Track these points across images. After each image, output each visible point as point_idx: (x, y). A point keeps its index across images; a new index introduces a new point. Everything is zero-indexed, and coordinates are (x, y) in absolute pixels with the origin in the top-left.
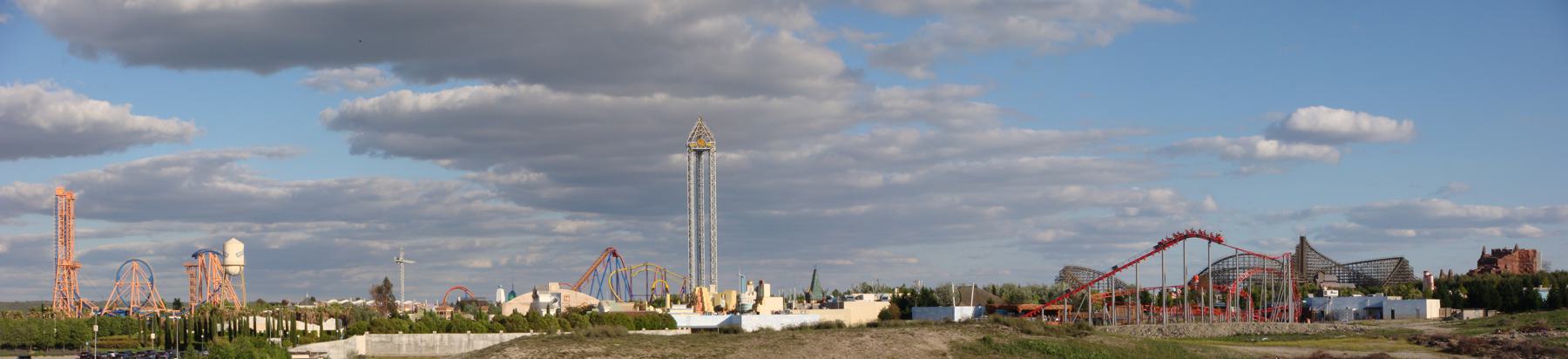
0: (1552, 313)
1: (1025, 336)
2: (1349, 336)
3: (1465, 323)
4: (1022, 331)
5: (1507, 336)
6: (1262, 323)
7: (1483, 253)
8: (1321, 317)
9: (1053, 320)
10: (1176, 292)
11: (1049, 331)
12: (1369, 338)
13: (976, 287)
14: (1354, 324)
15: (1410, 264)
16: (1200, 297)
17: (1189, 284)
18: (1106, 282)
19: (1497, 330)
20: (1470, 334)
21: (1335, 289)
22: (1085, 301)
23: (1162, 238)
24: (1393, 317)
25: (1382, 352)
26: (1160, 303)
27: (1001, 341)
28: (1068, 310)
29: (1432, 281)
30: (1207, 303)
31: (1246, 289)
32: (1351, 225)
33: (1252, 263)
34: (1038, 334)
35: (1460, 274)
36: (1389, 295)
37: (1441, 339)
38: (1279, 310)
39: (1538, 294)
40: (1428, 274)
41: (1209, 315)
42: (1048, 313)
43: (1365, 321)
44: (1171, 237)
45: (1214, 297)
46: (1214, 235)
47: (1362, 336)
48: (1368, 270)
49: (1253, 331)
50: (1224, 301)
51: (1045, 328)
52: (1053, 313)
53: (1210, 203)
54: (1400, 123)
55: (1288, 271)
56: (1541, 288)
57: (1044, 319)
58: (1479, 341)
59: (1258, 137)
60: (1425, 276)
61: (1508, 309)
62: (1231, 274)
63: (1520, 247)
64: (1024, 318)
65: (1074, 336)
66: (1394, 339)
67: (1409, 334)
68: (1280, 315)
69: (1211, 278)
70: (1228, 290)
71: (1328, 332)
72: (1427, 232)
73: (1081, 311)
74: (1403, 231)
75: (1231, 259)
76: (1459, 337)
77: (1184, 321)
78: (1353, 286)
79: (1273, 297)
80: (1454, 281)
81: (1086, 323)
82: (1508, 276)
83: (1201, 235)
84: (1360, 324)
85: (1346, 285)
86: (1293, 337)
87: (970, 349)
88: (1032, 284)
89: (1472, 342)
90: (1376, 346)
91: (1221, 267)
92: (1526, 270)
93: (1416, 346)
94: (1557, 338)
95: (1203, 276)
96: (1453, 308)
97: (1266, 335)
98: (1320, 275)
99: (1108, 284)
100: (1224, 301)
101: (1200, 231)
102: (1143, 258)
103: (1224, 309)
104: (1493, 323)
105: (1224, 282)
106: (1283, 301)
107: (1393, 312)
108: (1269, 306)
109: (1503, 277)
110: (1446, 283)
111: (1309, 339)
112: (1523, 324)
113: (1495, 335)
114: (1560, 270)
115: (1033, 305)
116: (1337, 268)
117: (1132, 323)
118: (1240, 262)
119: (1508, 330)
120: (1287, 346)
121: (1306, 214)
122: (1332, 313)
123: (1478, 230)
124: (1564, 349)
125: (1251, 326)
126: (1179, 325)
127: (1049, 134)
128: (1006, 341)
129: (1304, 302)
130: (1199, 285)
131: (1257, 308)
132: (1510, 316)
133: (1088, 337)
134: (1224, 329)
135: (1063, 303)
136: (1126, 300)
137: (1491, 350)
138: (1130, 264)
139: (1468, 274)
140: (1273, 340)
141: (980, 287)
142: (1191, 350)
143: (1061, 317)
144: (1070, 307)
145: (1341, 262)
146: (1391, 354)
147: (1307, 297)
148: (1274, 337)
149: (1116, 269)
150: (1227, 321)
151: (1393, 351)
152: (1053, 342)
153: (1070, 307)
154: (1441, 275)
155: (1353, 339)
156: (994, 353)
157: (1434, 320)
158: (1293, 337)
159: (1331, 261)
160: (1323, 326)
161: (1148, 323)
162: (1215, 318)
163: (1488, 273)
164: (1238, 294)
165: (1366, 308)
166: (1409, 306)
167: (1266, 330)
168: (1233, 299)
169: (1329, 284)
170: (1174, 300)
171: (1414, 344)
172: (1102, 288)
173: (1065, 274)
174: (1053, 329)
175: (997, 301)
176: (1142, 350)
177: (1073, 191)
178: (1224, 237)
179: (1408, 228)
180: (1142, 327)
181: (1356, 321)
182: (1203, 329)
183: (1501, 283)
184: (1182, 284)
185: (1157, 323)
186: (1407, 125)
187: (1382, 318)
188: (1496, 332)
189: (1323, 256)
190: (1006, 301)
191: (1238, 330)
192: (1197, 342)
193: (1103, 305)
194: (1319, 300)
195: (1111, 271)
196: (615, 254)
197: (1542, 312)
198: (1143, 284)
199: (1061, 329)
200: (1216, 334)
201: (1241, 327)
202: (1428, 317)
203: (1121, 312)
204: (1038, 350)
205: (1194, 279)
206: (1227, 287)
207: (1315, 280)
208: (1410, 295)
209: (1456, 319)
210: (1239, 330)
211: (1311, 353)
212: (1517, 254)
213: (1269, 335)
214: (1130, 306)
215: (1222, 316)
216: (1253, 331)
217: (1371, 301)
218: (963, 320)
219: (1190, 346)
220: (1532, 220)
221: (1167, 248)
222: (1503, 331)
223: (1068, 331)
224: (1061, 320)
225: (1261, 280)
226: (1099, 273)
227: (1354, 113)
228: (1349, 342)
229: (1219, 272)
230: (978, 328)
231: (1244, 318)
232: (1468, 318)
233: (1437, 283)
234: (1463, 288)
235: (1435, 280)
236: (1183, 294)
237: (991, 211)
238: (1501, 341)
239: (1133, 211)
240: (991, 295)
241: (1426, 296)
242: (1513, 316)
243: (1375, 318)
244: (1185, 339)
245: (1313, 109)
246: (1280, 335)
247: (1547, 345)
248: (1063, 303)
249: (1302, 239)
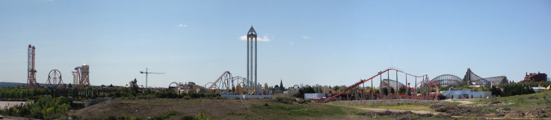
75: (441, 77)
102: (374, 77)
107: (472, 96)
196: (229, 73)
226: (481, 78)
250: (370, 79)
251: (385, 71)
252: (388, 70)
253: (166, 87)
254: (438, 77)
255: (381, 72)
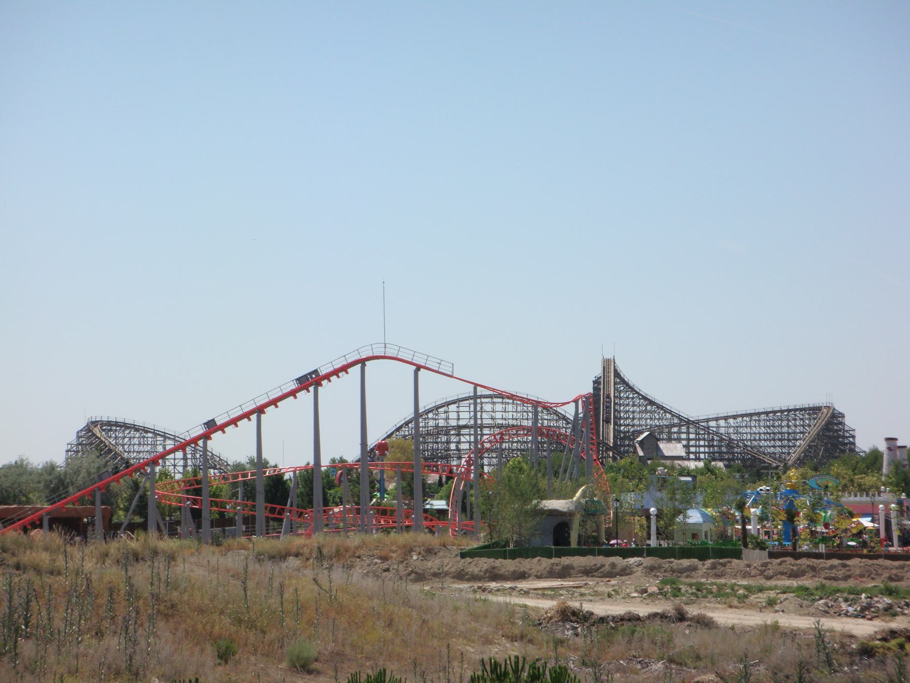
75: (453, 407)
102: (274, 402)
226: (679, 417)
250: (247, 415)
251: (345, 368)
252: (362, 362)
253: (37, 459)
254: (438, 408)
255: (316, 372)
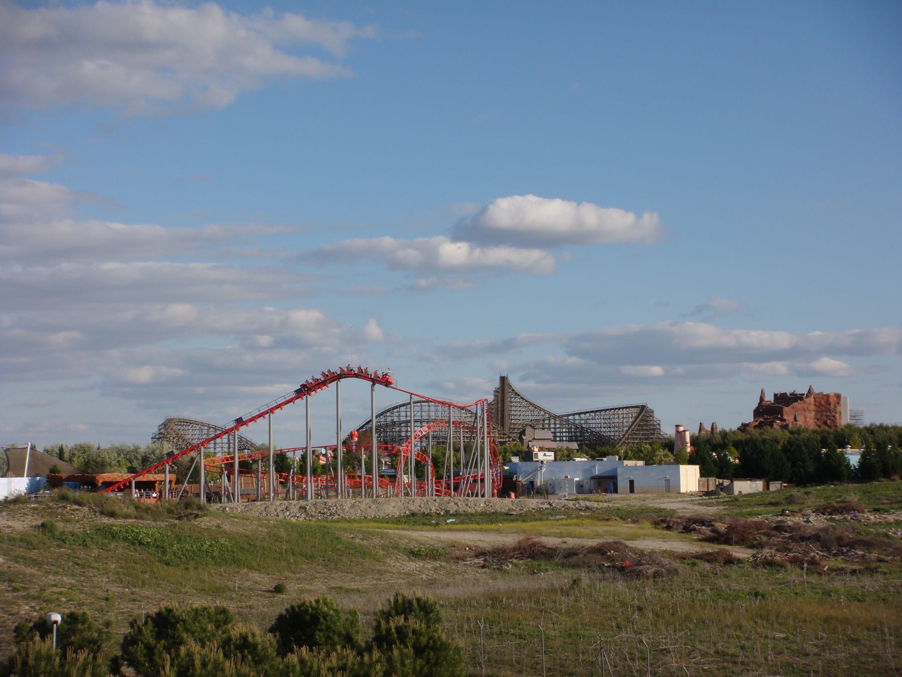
0: (867, 486)
1: (106, 520)
2: (569, 516)
3: (736, 500)
4: (102, 513)
5: (798, 519)
6: (447, 498)
7: (762, 399)
8: (531, 489)
9: (148, 496)
10: (325, 455)
11: (142, 511)
12: (598, 519)
13: (33, 448)
14: (576, 500)
15: (655, 414)
16: (360, 461)
17: (344, 443)
18: (226, 441)
19: (783, 511)
20: (743, 515)
21: (549, 450)
22: (195, 468)
23: (307, 378)
24: (632, 490)
25: (617, 539)
26: (302, 470)
27: (69, 528)
28: (170, 482)
29: (688, 440)
30: (369, 470)
31: (424, 451)
32: (573, 360)
33: (432, 414)
34: (127, 517)
35: (727, 430)
36: (625, 459)
37: (702, 522)
38: (471, 479)
39: (845, 459)
40: (681, 429)
41: (372, 488)
42: (140, 485)
43: (592, 496)
44: (319, 376)
45: (380, 462)
46: (380, 374)
47: (588, 517)
48: (597, 424)
49: (433, 510)
50: (393, 466)
51: (137, 508)
52: (148, 486)
53: (373, 330)
54: (639, 216)
55: (483, 425)
56: (849, 449)
57: (135, 494)
58: (758, 526)
59: (441, 238)
60: (678, 432)
61: (800, 479)
62: (404, 429)
63: (817, 390)
64: (105, 494)
65: (179, 518)
66: (634, 522)
67: (654, 515)
68: (472, 488)
69: (375, 436)
70: (399, 451)
71: (540, 511)
72: (679, 370)
73: (189, 483)
74: (646, 367)
75: (403, 409)
76: (728, 520)
77: (337, 496)
78: (574, 446)
79: (462, 461)
80: (719, 439)
81: (195, 500)
82: (799, 432)
83: (361, 374)
84: (585, 499)
85: (565, 445)
86: (490, 517)
87: (21, 540)
88: (117, 444)
89: (747, 527)
90: (606, 532)
91: (389, 419)
92: (825, 423)
93: (665, 532)
94: (875, 524)
95: (364, 432)
96: (718, 477)
97: (452, 516)
98: (529, 430)
99: (229, 443)
100: (393, 466)
101: (360, 369)
102: (279, 406)
103: (393, 478)
104: (776, 500)
105: (393, 440)
106: (476, 467)
107: (632, 483)
108: (457, 474)
109: (792, 433)
110: (708, 441)
111: (512, 521)
112: (823, 502)
113: (780, 518)
114: (878, 423)
115: (120, 475)
116: (552, 421)
117: (263, 499)
118: (416, 412)
119: (801, 510)
120: (481, 530)
121: (508, 345)
122: (546, 483)
123: (754, 366)
124: (886, 540)
125: (431, 503)
126: (330, 502)
127: (144, 229)
128: (77, 529)
129: (506, 468)
130: (359, 445)
131: (439, 478)
132: (803, 490)
133: (199, 519)
134: (394, 506)
135: (163, 471)
136: (254, 466)
137: (774, 540)
138: (261, 415)
139: (739, 429)
140: (462, 523)
141: (40, 449)
142: (346, 537)
143: (160, 492)
144: (174, 477)
145: (559, 412)
146: (630, 544)
147: (510, 461)
148: (465, 518)
149: (240, 422)
150: (397, 496)
151: (633, 538)
152: (148, 528)
153: (174, 477)
154: (700, 430)
155: (575, 521)
156: (59, 546)
157: (692, 495)
158: (490, 517)
159: (544, 410)
160: (532, 503)
161: (285, 499)
162: (381, 491)
163: (769, 428)
164: (414, 457)
165: (593, 478)
166: (656, 473)
167: (452, 508)
168: (406, 464)
169: (541, 443)
170: (323, 466)
171: (663, 528)
172: (220, 449)
173: (167, 430)
174: (147, 509)
175: (65, 470)
176: (277, 538)
177: (181, 311)
178: (393, 378)
179: (655, 363)
180: (277, 504)
181: (580, 496)
182: (363, 507)
183: (789, 442)
184: (333, 442)
185: (299, 499)
186: (650, 220)
187: (616, 491)
188: (783, 513)
189: (531, 404)
190: (78, 469)
191: (412, 508)
192: (356, 525)
193: (221, 473)
194: (527, 466)
195: (233, 425)
197: (851, 486)
198: (279, 443)
199: (161, 509)
200: (381, 515)
201: (417, 504)
202: (683, 490)
203: (246, 484)
204: (126, 539)
205: (351, 436)
206: (397, 447)
207: (521, 440)
208: (657, 459)
209: (723, 494)
210: (414, 508)
211: (517, 540)
212: (811, 399)
213: (456, 515)
214: (260, 475)
215: (390, 488)
216: (433, 510)
217: (600, 467)
218: (11, 498)
219: (345, 530)
220: (833, 351)
221: (313, 393)
222: (791, 511)
223: (170, 511)
224: (160, 496)
225: (446, 438)
226: (215, 428)
227: (574, 204)
228: (570, 525)
229: (387, 426)
230: (33, 509)
231: (422, 492)
232: (740, 492)
233: (695, 441)
234: (733, 449)
235: (691, 438)
236: (335, 457)
237: (59, 338)
238: (789, 527)
239: (265, 340)
240: (56, 461)
241: (680, 460)
242: (808, 490)
243: (606, 491)
244: (338, 521)
245: (518, 199)
246: (472, 514)
247: (859, 533)
248: (163, 471)
249: (503, 380)
